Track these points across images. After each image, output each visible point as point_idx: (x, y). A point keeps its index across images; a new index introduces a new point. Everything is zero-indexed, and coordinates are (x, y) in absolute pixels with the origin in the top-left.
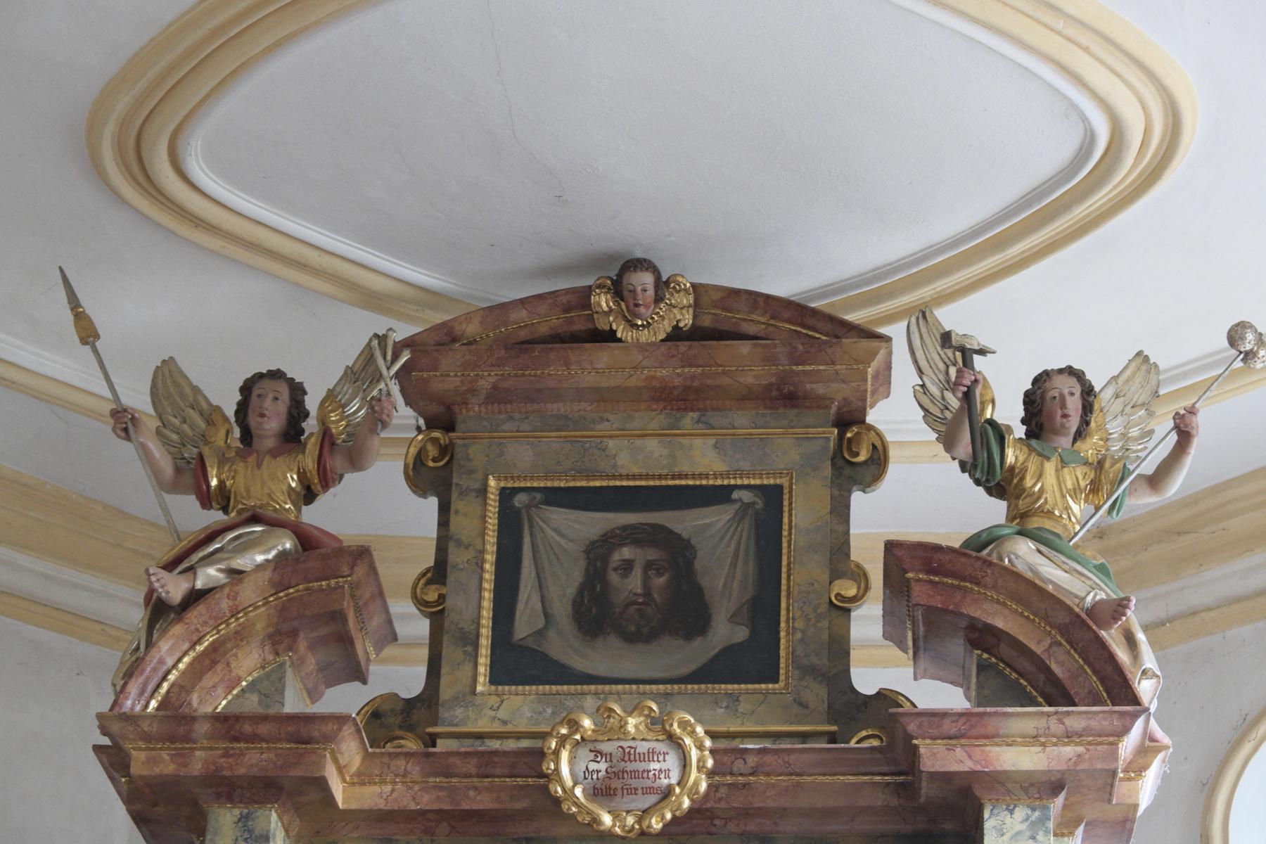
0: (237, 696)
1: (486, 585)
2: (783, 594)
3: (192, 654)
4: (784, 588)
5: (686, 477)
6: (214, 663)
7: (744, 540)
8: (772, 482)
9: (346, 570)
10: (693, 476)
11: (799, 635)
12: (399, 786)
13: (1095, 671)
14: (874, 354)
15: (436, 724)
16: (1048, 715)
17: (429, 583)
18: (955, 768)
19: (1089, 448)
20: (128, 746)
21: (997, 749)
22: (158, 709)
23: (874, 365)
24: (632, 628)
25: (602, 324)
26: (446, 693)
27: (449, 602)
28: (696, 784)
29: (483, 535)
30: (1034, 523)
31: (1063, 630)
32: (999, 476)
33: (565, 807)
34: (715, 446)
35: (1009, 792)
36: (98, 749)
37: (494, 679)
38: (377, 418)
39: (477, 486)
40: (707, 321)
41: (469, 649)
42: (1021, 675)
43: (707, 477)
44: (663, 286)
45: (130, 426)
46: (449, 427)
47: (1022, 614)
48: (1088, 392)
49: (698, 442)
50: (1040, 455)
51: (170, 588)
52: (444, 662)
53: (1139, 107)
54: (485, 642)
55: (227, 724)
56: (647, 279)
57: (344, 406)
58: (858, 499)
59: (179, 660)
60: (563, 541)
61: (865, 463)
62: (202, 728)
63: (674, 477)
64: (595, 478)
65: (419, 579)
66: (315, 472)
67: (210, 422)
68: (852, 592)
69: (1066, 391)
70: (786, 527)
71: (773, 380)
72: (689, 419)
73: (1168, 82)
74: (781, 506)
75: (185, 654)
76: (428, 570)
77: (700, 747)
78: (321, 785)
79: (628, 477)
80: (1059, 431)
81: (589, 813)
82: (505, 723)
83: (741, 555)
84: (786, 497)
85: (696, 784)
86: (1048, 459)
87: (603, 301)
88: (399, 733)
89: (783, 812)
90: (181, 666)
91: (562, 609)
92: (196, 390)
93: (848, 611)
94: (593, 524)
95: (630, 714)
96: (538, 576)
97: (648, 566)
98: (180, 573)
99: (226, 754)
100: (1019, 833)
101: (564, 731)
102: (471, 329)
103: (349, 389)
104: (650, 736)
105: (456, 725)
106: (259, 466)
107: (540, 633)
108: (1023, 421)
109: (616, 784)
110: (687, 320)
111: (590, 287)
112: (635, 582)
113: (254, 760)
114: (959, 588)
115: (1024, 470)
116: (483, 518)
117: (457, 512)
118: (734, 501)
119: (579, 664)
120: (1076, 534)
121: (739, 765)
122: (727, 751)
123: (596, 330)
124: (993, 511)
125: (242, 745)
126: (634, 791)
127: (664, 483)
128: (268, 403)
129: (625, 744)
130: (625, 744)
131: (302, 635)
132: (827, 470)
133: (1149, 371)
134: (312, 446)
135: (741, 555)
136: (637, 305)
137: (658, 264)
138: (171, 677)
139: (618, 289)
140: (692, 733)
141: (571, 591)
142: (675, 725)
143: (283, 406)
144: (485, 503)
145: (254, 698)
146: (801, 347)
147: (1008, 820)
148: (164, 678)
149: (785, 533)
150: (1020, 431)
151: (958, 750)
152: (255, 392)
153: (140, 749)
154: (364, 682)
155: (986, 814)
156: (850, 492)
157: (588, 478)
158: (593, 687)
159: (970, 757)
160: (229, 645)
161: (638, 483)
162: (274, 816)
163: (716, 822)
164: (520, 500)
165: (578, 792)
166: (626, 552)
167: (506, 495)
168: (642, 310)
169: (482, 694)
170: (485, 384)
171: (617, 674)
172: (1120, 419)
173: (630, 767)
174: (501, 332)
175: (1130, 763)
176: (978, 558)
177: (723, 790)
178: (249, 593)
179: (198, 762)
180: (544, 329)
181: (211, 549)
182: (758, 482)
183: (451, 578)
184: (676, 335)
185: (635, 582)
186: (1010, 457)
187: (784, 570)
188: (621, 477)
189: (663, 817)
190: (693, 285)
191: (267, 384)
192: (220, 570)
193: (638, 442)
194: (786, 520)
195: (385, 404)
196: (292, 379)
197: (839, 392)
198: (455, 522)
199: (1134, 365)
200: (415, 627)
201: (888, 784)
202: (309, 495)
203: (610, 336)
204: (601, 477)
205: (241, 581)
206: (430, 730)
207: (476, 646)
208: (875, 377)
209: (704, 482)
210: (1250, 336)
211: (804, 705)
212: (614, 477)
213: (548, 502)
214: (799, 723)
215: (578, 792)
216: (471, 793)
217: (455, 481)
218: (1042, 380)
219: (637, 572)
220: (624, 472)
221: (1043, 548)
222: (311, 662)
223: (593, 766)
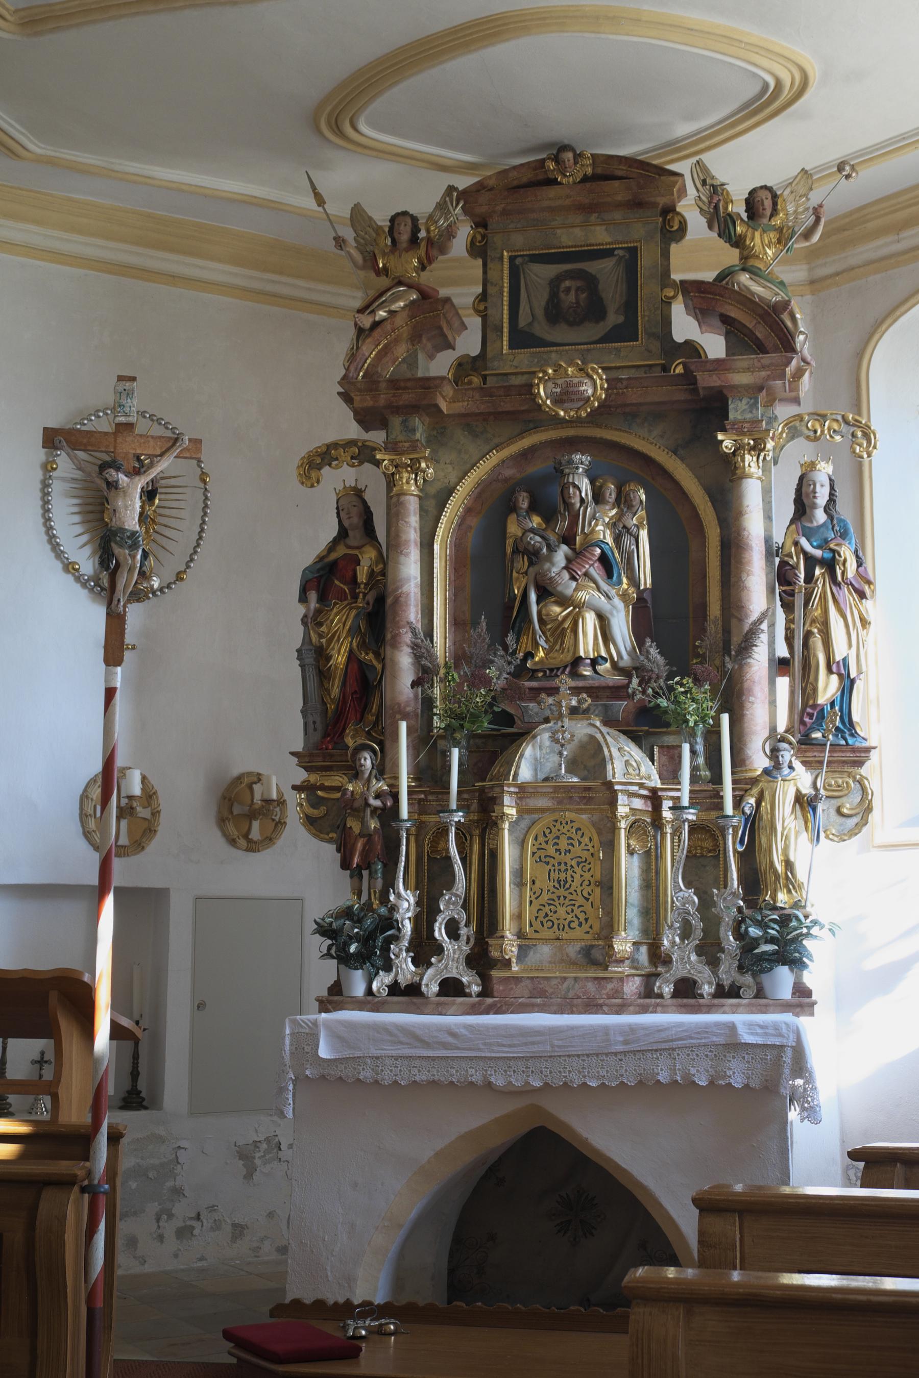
0: (398, 365)
1: (505, 303)
2: (639, 299)
3: (376, 350)
4: (639, 296)
5: (593, 245)
6: (386, 353)
7: (620, 275)
8: (632, 245)
9: (440, 308)
10: (596, 245)
11: (647, 318)
12: (470, 402)
13: (776, 335)
14: (677, 182)
15: (486, 370)
16: (753, 359)
17: (480, 301)
18: (712, 384)
19: (777, 221)
20: (352, 395)
21: (731, 375)
22: (363, 377)
23: (677, 187)
24: (571, 319)
25: (551, 176)
26: (490, 354)
27: (489, 312)
28: (601, 394)
29: (502, 279)
30: (752, 262)
31: (761, 316)
32: (734, 239)
33: (543, 408)
34: (606, 230)
35: (739, 392)
36: (339, 393)
37: (511, 347)
38: (449, 233)
39: (498, 255)
40: (599, 171)
41: (499, 333)
42: (745, 335)
43: (603, 244)
44: (578, 157)
45: (342, 244)
46: (485, 226)
47: (742, 310)
48: (775, 197)
49: (598, 228)
50: (752, 228)
51: (364, 322)
52: (488, 340)
53: (786, 70)
54: (506, 330)
55: (395, 383)
56: (570, 155)
57: (436, 222)
58: (674, 247)
59: (371, 353)
60: (539, 280)
61: (677, 230)
62: (383, 385)
63: (587, 246)
64: (551, 248)
65: (475, 300)
66: (425, 258)
67: (378, 234)
68: (672, 294)
69: (764, 198)
70: (639, 267)
71: (630, 197)
72: (593, 217)
73: (798, 61)
74: (637, 257)
75: (373, 350)
76: (479, 295)
77: (601, 379)
78: (437, 406)
79: (567, 247)
80: (763, 216)
81: (554, 411)
82: (516, 367)
83: (620, 280)
84: (639, 252)
85: (601, 394)
86: (757, 230)
87: (551, 165)
88: (471, 373)
89: (641, 404)
90: (372, 356)
91: (540, 312)
92: (370, 218)
93: (670, 303)
94: (552, 270)
95: (569, 367)
96: (528, 296)
97: (578, 289)
98: (369, 313)
99: (394, 396)
100: (744, 410)
101: (541, 375)
102: (491, 183)
103: (438, 214)
104: (579, 375)
105: (495, 370)
106: (400, 256)
107: (530, 324)
108: (746, 211)
109: (565, 397)
110: (590, 171)
111: (544, 159)
112: (572, 297)
113: (407, 398)
114: (714, 299)
115: (746, 236)
116: (502, 270)
117: (490, 269)
118: (616, 255)
119: (549, 338)
120: (771, 265)
121: (619, 385)
122: (613, 380)
123: (548, 178)
124: (732, 256)
125: (400, 391)
126: (572, 401)
127: (583, 248)
128: (402, 227)
129: (568, 380)
130: (568, 380)
131: (424, 336)
132: (658, 237)
133: (807, 178)
134: (423, 245)
135: (620, 280)
136: (566, 168)
137: (574, 145)
138: (368, 361)
139: (556, 159)
140: (597, 373)
141: (543, 303)
142: (589, 370)
143: (409, 228)
144: (502, 264)
145: (405, 366)
146: (642, 182)
147: (739, 404)
148: (365, 362)
149: (639, 270)
150: (744, 216)
151: (714, 376)
152: (396, 223)
153: (357, 395)
154: (454, 349)
155: (730, 402)
156: (670, 245)
157: (548, 249)
158: (555, 348)
159: (719, 379)
160: (392, 345)
161: (571, 249)
162: (417, 419)
163: (612, 409)
164: (518, 261)
165: (548, 402)
166: (567, 283)
167: (512, 259)
168: (568, 169)
169: (506, 354)
170: (499, 208)
171: (566, 341)
172: (793, 203)
173: (571, 389)
174: (427, 466)
175: (795, 374)
176: (721, 286)
177: (613, 396)
178: (399, 320)
179: (382, 401)
180: (525, 180)
181: (381, 301)
182: (626, 245)
183: (489, 300)
184: (585, 179)
185: (572, 297)
186: (739, 229)
187: (639, 287)
188: (563, 247)
189: (586, 411)
190: (591, 155)
191: (401, 218)
192: (385, 312)
193: (571, 230)
194: (639, 263)
195: (454, 228)
196: (412, 215)
197: (662, 201)
198: (490, 273)
199: (800, 175)
200: (474, 323)
201: (686, 389)
202: (423, 267)
203: (553, 182)
204: (554, 248)
205: (395, 316)
206: (483, 373)
207: (502, 332)
208: (679, 190)
209: (601, 247)
210: (847, 168)
211: (650, 351)
212: (560, 248)
213: (531, 261)
214: (645, 360)
215: (548, 402)
216: (502, 404)
217: (488, 254)
218: (753, 192)
219: (573, 293)
220: (564, 245)
221: (753, 277)
222: (429, 346)
223: (554, 390)
